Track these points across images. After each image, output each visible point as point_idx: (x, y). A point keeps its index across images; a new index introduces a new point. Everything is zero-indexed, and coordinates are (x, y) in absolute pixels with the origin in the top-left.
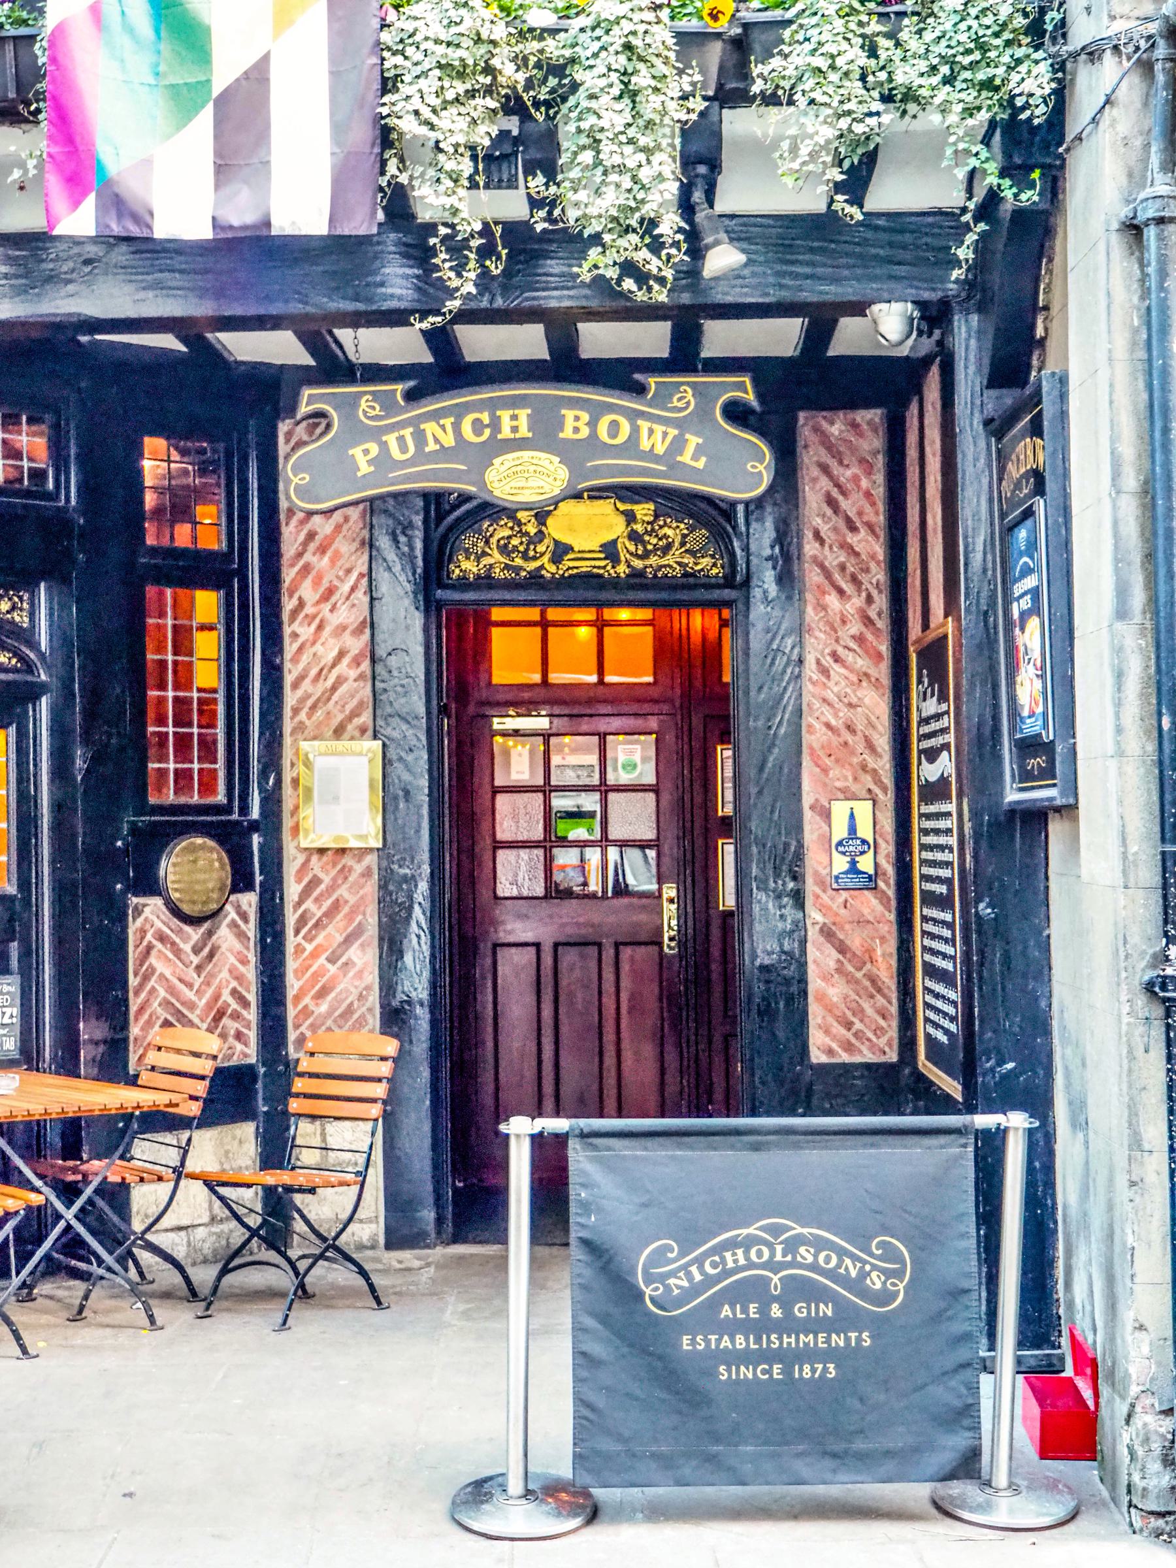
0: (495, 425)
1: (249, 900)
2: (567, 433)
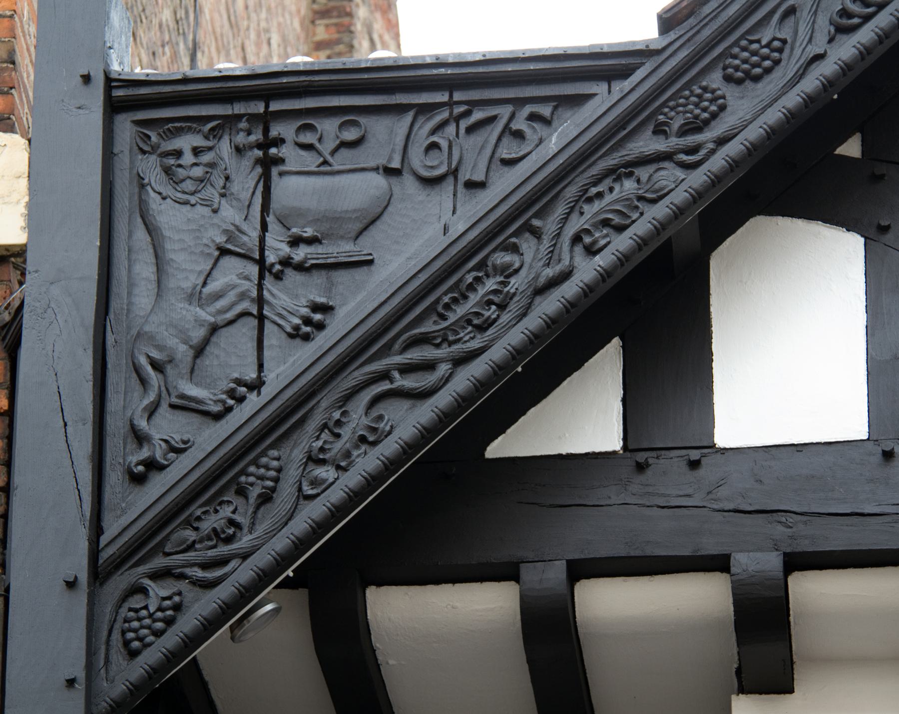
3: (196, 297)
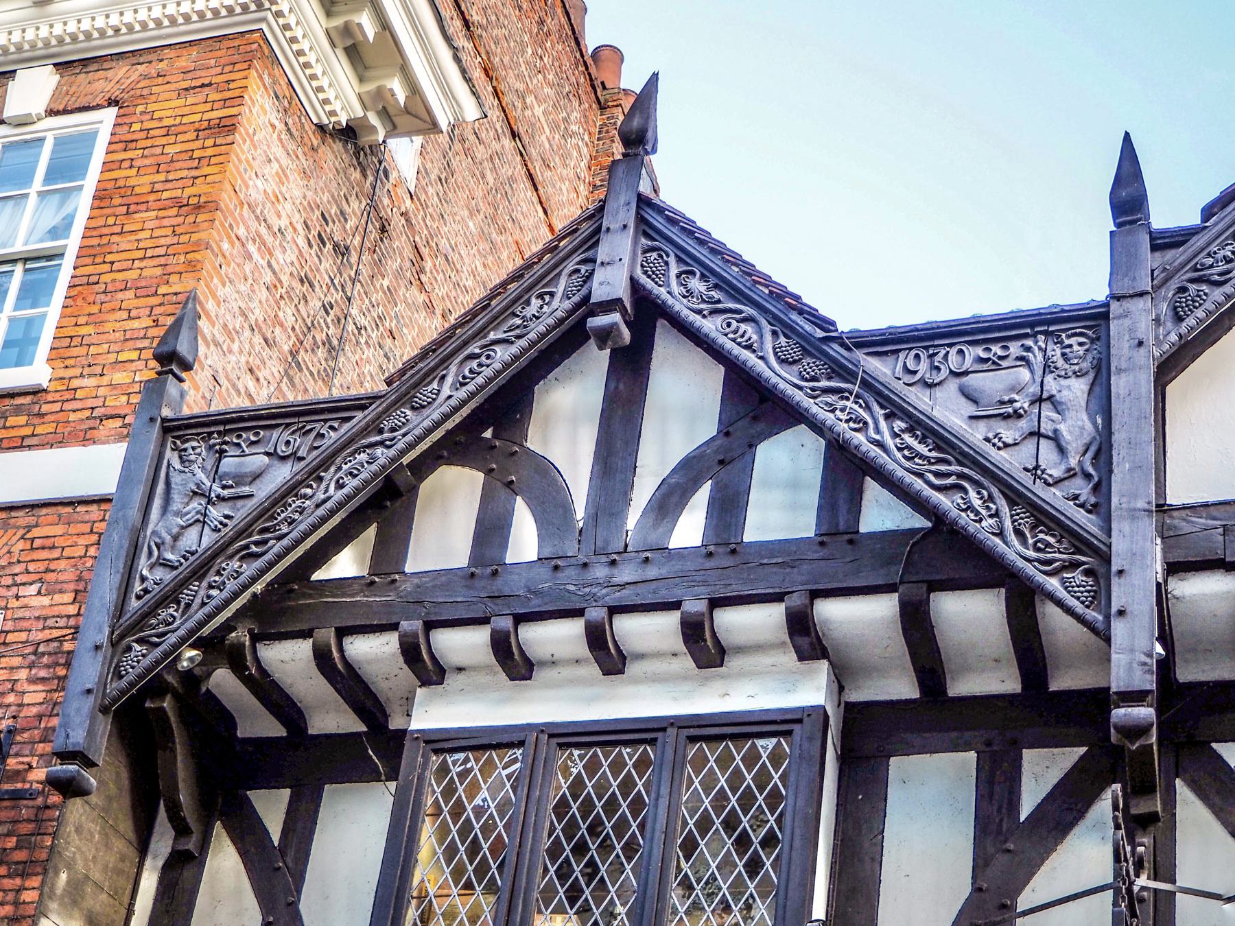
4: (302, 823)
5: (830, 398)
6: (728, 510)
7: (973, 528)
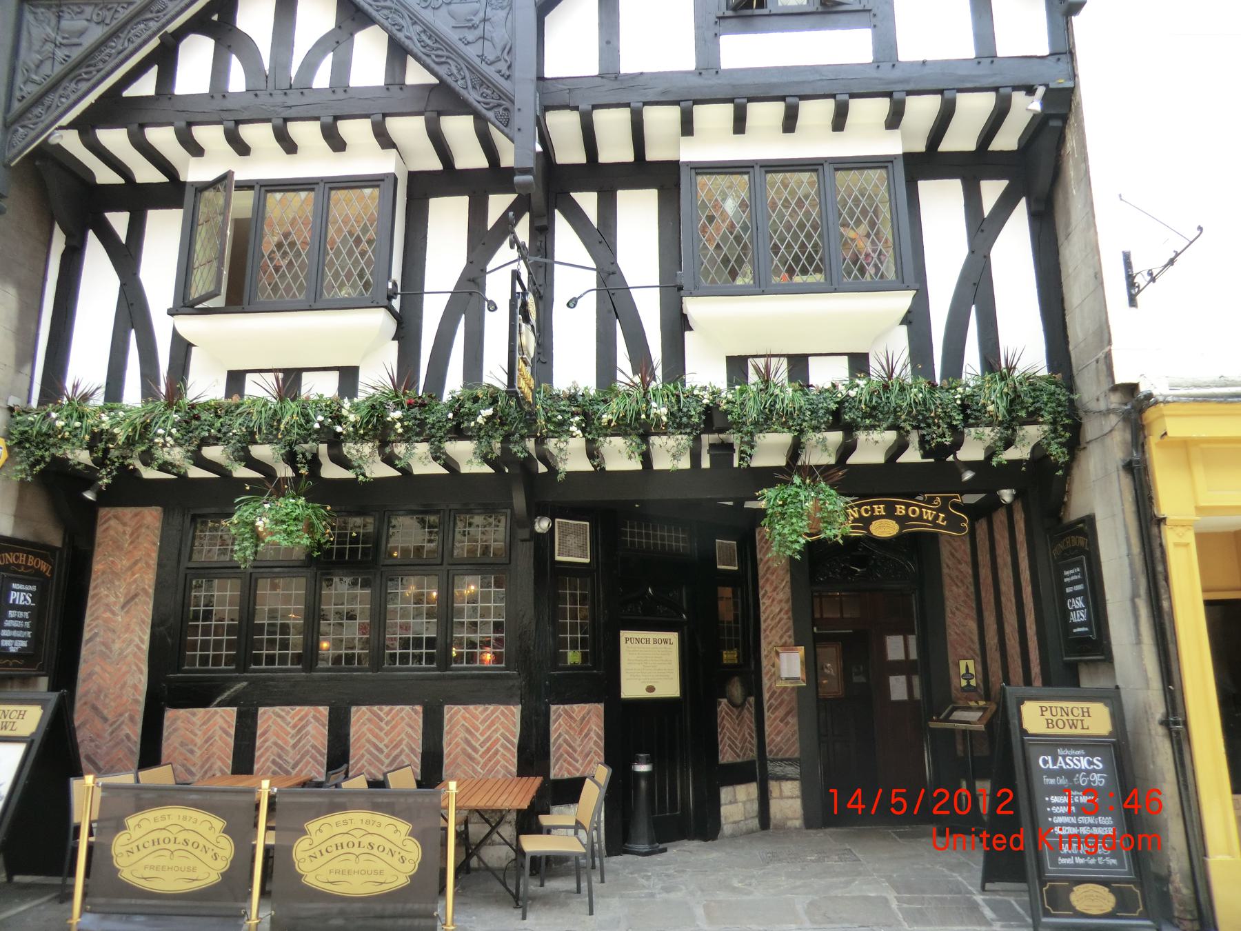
0: (873, 510)
1: (752, 699)
2: (898, 513)
3: (39, 52)
4: (137, 228)
5: (386, 12)
6: (342, 69)
7: (453, 84)
